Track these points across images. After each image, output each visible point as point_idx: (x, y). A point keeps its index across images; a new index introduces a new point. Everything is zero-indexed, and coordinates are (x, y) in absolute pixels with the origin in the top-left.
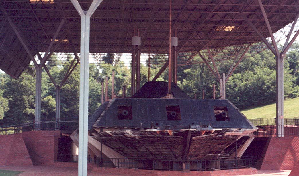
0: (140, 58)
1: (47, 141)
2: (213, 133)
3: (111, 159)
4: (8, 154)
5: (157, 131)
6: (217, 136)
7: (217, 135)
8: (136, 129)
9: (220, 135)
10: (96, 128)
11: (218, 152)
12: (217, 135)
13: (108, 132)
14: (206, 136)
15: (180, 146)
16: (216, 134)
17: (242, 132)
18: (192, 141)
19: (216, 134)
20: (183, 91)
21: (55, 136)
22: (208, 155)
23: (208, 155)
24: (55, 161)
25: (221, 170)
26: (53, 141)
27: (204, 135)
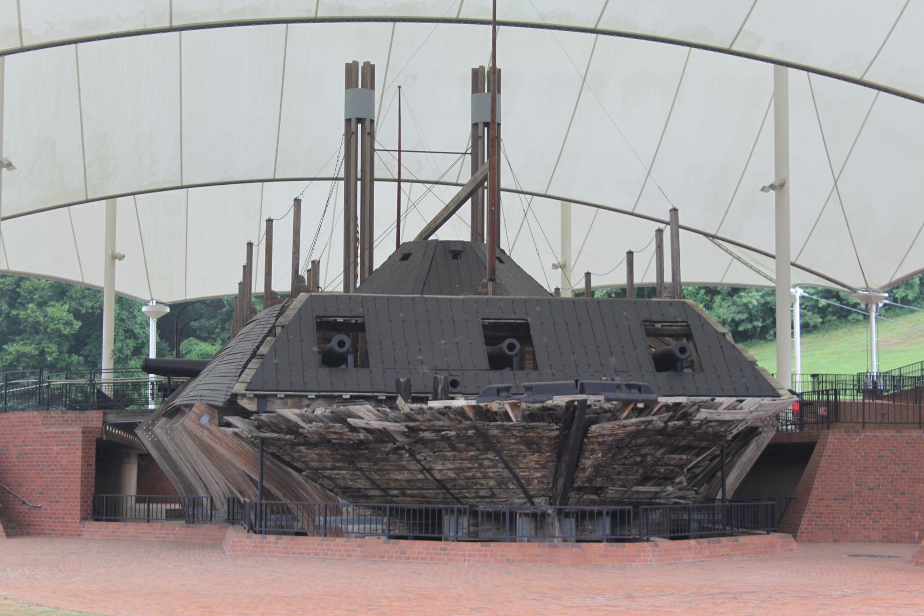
0: (472, 235)
1: (56, 449)
2: (654, 414)
3: (772, 332)
4: (836, 393)
5: (468, 406)
6: (671, 424)
7: (670, 420)
8: (381, 401)
9: (679, 420)
10: (244, 396)
11: (668, 479)
12: (670, 420)
13: (291, 414)
14: (634, 420)
15: (259, 352)
16: (666, 415)
17: (752, 407)
18: (588, 438)
19: (666, 415)
20: (574, 302)
21: (83, 433)
22: (634, 489)
23: (634, 489)
24: (84, 519)
25: (672, 539)
26: (77, 449)
27: (627, 418)
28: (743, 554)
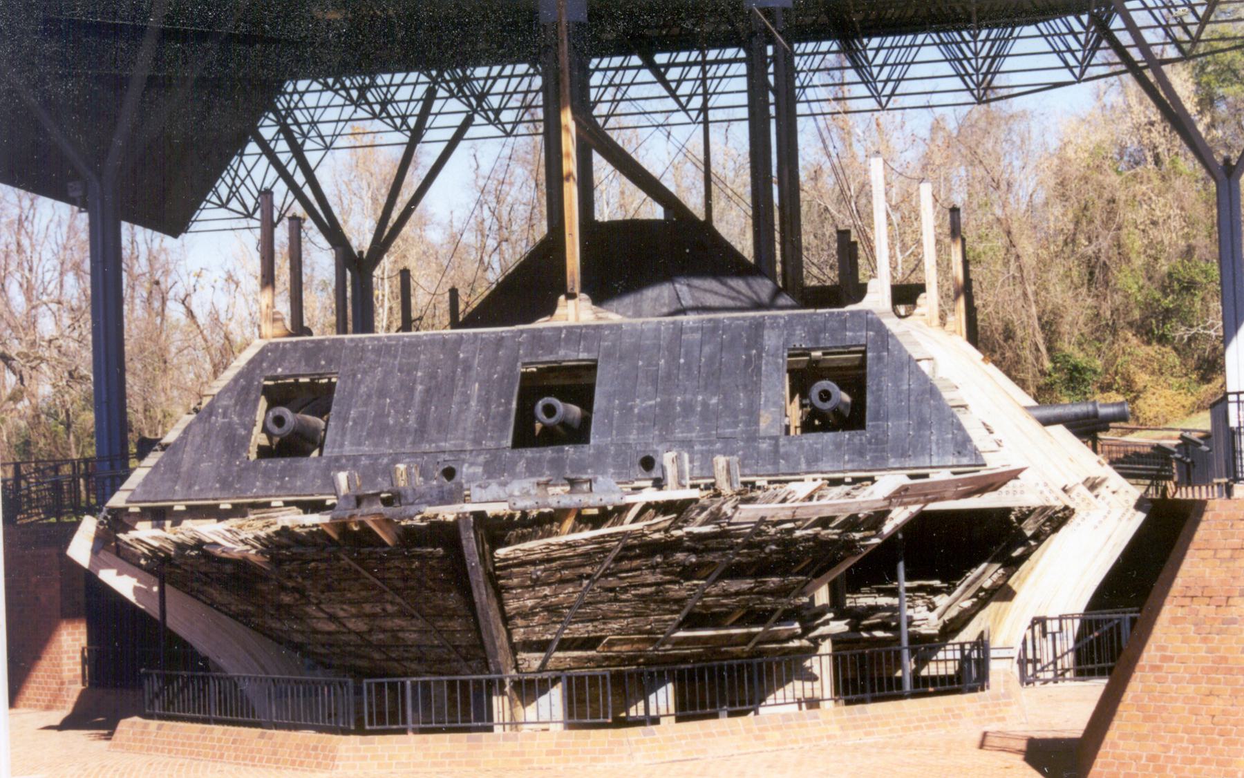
27: (573, 530)
28: (867, 734)
